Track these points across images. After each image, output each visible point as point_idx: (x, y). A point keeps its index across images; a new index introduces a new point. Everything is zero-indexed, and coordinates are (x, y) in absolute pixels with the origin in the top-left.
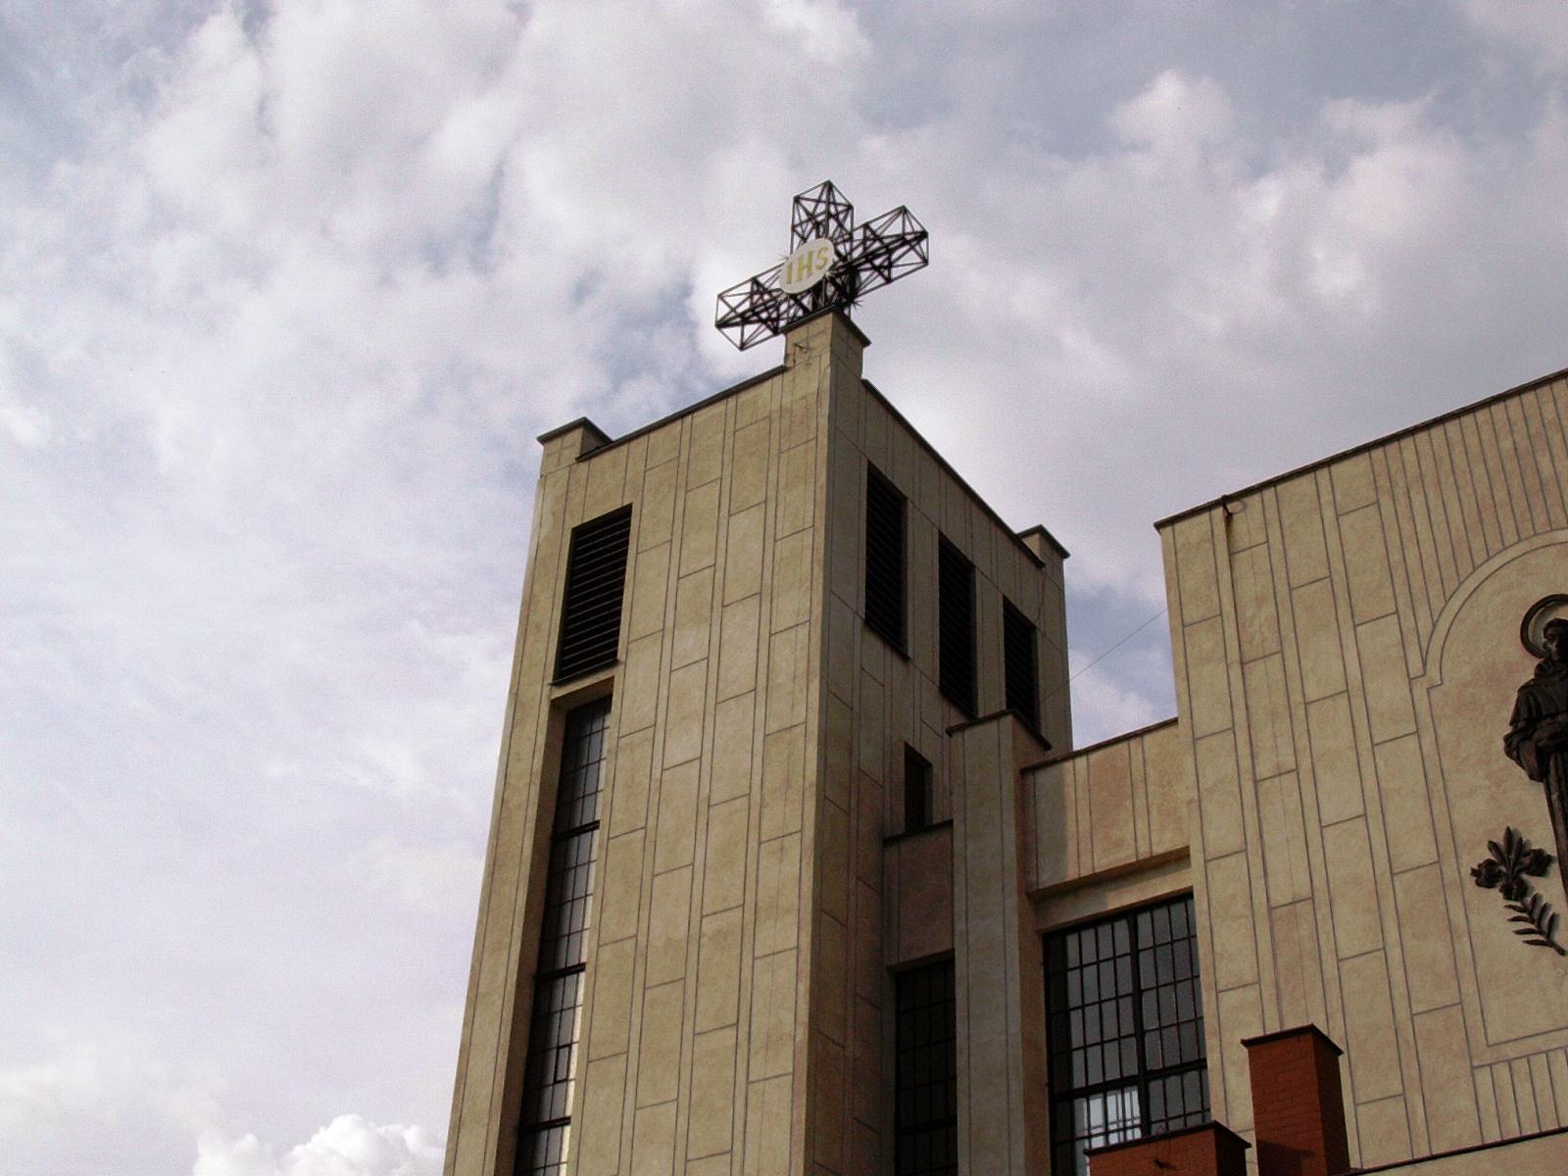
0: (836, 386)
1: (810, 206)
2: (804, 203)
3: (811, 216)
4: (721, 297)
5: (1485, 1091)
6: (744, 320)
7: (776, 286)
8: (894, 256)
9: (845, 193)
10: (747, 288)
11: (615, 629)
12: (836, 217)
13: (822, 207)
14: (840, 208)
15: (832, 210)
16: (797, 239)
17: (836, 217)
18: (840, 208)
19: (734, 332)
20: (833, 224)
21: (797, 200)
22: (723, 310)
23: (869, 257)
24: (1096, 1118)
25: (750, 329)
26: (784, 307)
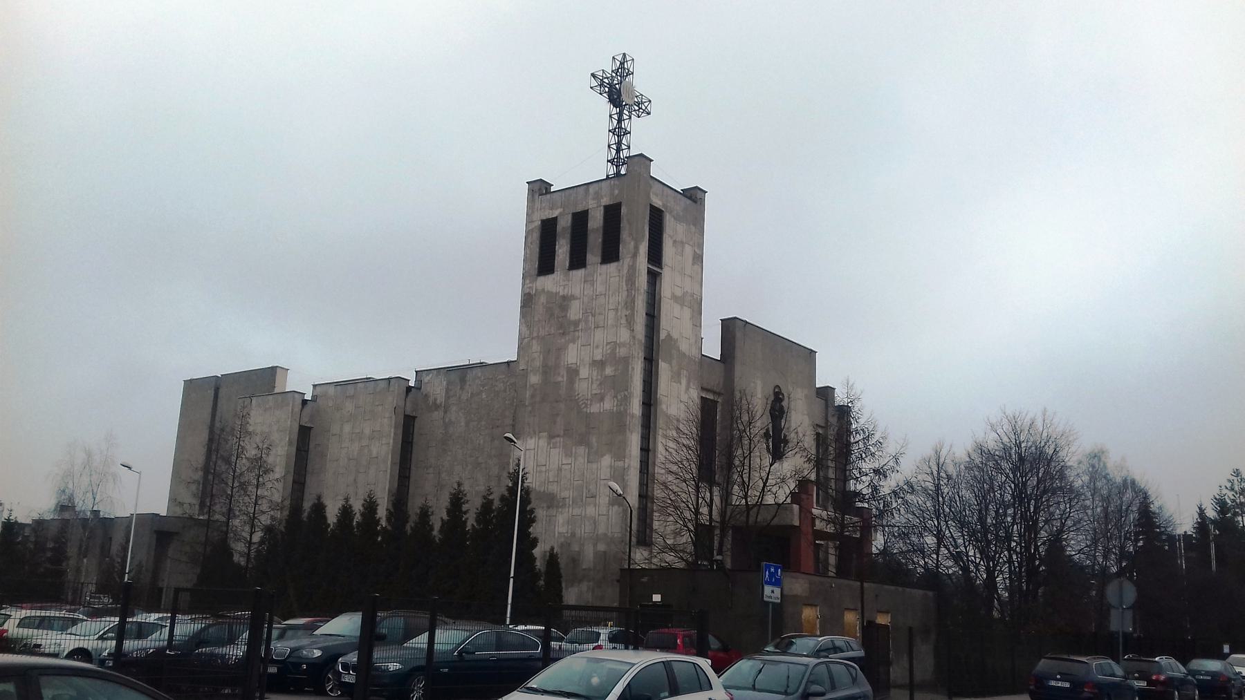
0: (669, 648)
1: (646, 104)
2: (647, 103)
3: (642, 103)
4: (633, 59)
5: (235, 652)
6: (622, 64)
7: (627, 79)
8: (616, 137)
9: (645, 118)
10: (628, 129)
11: (771, 606)
12: (638, 110)
13: (644, 108)
14: (640, 113)
15: (641, 110)
16: (638, 94)
17: (638, 110)
18: (640, 113)
19: (620, 58)
20: (637, 108)
21: (650, 101)
22: (628, 58)
23: (620, 128)
24: (127, 645)
25: (618, 63)
26: (619, 78)
